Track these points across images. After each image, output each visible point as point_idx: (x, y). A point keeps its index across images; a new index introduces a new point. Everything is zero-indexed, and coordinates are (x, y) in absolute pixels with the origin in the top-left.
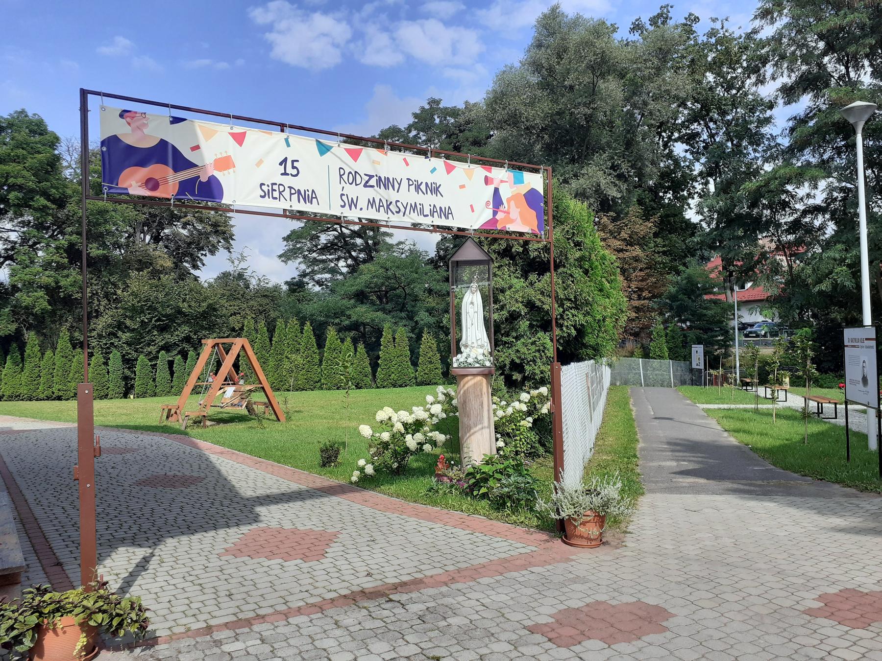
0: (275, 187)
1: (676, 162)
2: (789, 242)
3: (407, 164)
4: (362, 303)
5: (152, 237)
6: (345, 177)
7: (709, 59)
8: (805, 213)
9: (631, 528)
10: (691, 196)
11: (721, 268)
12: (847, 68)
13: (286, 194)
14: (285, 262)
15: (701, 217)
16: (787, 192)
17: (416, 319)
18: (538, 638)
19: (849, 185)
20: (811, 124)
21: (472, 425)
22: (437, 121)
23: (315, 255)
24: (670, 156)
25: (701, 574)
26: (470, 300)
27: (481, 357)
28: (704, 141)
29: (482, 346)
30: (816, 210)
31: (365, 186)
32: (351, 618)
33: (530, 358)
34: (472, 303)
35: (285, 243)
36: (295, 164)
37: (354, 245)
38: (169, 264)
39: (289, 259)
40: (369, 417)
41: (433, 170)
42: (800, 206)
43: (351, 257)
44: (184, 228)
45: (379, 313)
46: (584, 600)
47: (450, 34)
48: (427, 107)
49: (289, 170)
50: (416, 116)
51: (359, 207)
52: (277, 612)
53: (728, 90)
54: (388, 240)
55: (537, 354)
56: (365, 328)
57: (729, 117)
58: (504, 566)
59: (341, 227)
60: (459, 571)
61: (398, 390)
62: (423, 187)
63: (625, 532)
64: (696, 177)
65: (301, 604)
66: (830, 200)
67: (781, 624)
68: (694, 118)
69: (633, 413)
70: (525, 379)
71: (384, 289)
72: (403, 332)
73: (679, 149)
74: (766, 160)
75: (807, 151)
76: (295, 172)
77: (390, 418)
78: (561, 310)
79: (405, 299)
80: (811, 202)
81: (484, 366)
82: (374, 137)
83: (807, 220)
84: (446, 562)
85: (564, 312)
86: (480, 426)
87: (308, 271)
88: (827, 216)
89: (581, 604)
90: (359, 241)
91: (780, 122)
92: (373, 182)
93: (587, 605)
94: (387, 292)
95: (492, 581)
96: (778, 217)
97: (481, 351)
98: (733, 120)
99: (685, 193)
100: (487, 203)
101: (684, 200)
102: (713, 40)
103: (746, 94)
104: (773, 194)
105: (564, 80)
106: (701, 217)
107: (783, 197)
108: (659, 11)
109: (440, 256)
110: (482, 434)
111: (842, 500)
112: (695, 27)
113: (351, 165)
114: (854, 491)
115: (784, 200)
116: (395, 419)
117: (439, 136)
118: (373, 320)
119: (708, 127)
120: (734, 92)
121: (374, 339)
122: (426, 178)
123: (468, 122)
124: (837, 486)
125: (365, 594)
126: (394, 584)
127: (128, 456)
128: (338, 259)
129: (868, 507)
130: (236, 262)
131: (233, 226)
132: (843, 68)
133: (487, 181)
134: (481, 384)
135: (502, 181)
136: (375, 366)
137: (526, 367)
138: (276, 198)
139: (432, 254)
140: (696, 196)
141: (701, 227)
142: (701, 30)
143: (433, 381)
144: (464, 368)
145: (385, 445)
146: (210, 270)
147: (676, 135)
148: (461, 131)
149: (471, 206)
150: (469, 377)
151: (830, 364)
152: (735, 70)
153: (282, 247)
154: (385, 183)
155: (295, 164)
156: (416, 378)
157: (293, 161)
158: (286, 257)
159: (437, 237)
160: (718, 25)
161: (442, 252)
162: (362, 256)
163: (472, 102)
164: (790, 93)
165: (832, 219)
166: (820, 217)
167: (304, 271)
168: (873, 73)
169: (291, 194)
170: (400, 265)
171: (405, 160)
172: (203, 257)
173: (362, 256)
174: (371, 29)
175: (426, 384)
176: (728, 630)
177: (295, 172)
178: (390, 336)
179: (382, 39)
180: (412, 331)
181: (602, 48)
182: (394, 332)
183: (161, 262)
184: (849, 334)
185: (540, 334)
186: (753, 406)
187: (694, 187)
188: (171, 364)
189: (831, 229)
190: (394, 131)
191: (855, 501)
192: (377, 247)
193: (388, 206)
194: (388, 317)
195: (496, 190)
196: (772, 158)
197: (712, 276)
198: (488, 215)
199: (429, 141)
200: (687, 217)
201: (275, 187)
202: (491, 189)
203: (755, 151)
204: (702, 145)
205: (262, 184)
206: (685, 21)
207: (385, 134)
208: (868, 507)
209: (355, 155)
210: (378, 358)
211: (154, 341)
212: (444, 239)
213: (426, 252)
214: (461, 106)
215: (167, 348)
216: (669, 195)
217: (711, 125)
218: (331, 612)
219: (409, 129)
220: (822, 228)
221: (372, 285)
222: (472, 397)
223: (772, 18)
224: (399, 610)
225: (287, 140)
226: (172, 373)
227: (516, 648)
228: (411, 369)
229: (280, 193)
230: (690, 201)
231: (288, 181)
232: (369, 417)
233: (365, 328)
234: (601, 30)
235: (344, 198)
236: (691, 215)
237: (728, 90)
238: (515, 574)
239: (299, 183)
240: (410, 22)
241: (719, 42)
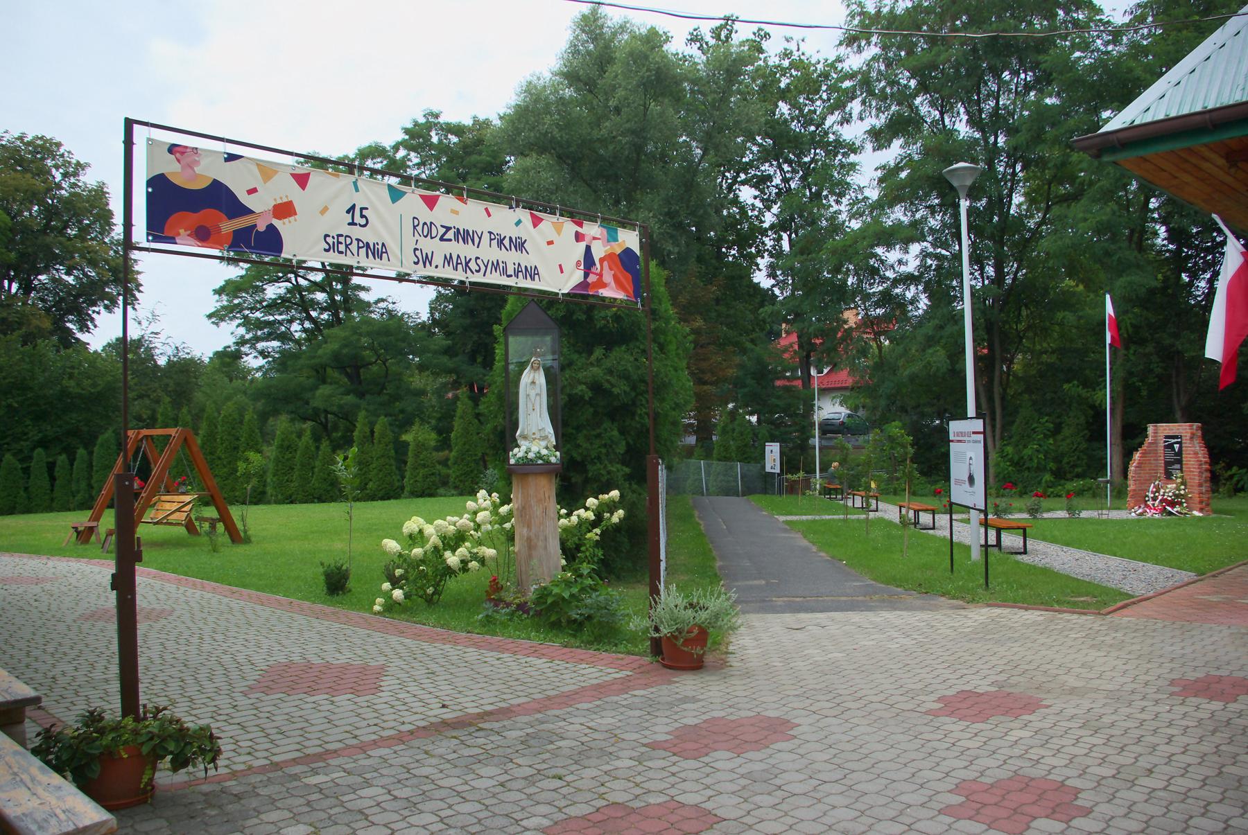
0: (342, 239)
1: (743, 209)
2: (878, 317)
3: (489, 215)
5: (20, 285)
6: (419, 228)
7: (782, 85)
8: (896, 282)
9: (731, 648)
10: (760, 254)
11: (796, 347)
12: (942, 114)
13: (354, 247)
14: (217, 324)
15: (773, 282)
16: (875, 256)
18: (662, 753)
19: (944, 252)
20: (903, 175)
22: (435, 139)
23: (258, 314)
24: (736, 201)
25: (818, 687)
27: (544, 452)
28: (777, 186)
29: (545, 438)
30: (908, 279)
31: (442, 239)
32: (444, 746)
33: (593, 454)
34: (533, 383)
35: (217, 297)
36: (365, 212)
37: (314, 304)
38: (47, 324)
39: (222, 320)
40: (394, 531)
41: (518, 223)
42: (890, 274)
43: (309, 318)
44: (68, 273)
45: (350, 398)
46: (593, 803)
49: (358, 219)
50: (407, 131)
51: (434, 264)
52: (348, 747)
53: (805, 125)
54: (363, 296)
55: (604, 451)
57: (807, 159)
58: (600, 690)
59: (297, 276)
60: (549, 698)
62: (506, 242)
63: (727, 653)
64: (766, 230)
65: (374, 737)
66: (924, 268)
67: (905, 725)
68: (766, 155)
69: (702, 527)
70: (587, 481)
73: (747, 194)
74: (852, 216)
75: (897, 208)
76: (363, 221)
78: (633, 394)
80: (903, 269)
81: (548, 463)
82: (346, 157)
83: (898, 291)
84: (531, 691)
87: (248, 337)
88: (920, 288)
89: (696, 721)
90: (320, 296)
91: (868, 170)
92: (450, 235)
93: (705, 721)
95: (590, 705)
96: (866, 286)
97: (544, 443)
98: (811, 162)
99: (753, 250)
100: (578, 263)
101: (751, 259)
102: (786, 63)
103: (826, 133)
104: (858, 252)
105: (607, 100)
106: (773, 282)
107: (872, 262)
109: (434, 320)
111: (950, 612)
112: (765, 45)
113: (425, 215)
114: (961, 602)
115: (873, 267)
117: (438, 159)
118: (341, 407)
119: (781, 170)
120: (813, 128)
122: (510, 231)
124: (943, 599)
125: (445, 724)
126: (478, 714)
127: (48, 586)
128: (291, 321)
129: (977, 617)
130: (145, 324)
131: (139, 273)
132: (937, 113)
133: (579, 237)
135: (595, 238)
137: (589, 467)
138: (341, 253)
139: (425, 316)
140: (766, 254)
141: (773, 294)
142: (773, 51)
146: (102, 331)
147: (743, 176)
149: (560, 266)
151: (932, 463)
152: (813, 101)
153: (214, 303)
154: (465, 236)
155: (365, 212)
157: (362, 209)
158: (218, 317)
159: (431, 292)
160: (792, 46)
161: (437, 315)
162: (325, 316)
163: (482, 117)
164: (880, 138)
165: (925, 291)
166: (912, 288)
167: (243, 336)
168: (967, 121)
169: (359, 248)
171: (486, 210)
172: (95, 316)
173: (325, 316)
176: (854, 733)
177: (363, 221)
181: (657, 63)
183: (35, 322)
184: (955, 427)
185: (607, 424)
186: (842, 517)
187: (763, 243)
188: (51, 467)
189: (924, 302)
190: (375, 151)
191: (963, 612)
193: (467, 264)
195: (588, 248)
196: (859, 214)
197: (786, 356)
198: (578, 276)
200: (756, 280)
201: (342, 239)
202: (583, 245)
203: (837, 202)
204: (775, 191)
205: (327, 236)
206: (753, 37)
207: (364, 154)
208: (977, 617)
209: (431, 202)
211: (25, 434)
212: (440, 297)
215: (44, 443)
216: (733, 252)
217: (786, 167)
218: (415, 743)
219: (396, 148)
220: (914, 301)
223: (859, 47)
224: (495, 738)
225: (355, 183)
226: (53, 479)
227: (640, 763)
229: (347, 246)
230: (759, 260)
231: (356, 232)
232: (394, 531)
234: (653, 40)
235: (418, 253)
236: (761, 278)
237: (805, 125)
238: (615, 698)
239: (367, 235)
241: (793, 65)
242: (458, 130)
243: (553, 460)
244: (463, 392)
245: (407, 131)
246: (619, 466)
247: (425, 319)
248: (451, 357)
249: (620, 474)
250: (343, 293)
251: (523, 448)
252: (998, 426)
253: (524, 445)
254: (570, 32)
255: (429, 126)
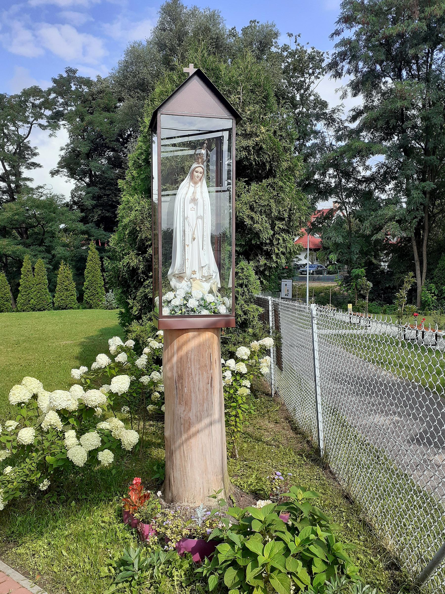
4: (5, 237)
17: (53, 252)
21: (193, 418)
22: (73, 88)
26: (190, 195)
29: (208, 279)
45: (20, 247)
47: (79, 39)
48: (65, 75)
54: (28, 183)
56: (6, 259)
61: (37, 314)
71: (24, 225)
72: (41, 264)
77: (35, 397)
78: (272, 232)
79: (44, 235)
81: (216, 314)
85: (274, 234)
86: (206, 421)
94: (27, 229)
97: (207, 286)
108: (249, 24)
109: (74, 202)
110: (210, 434)
116: (44, 401)
117: (75, 100)
118: (14, 252)
121: (15, 269)
123: (100, 92)
134: (210, 347)
136: (15, 292)
139: (68, 199)
143: (69, 305)
144: (182, 316)
145: (25, 450)
148: (94, 99)
150: (191, 334)
156: (53, 303)
161: (76, 199)
170: (39, 205)
174: (17, 25)
175: (63, 309)
178: (30, 267)
179: (26, 35)
180: (49, 263)
182: (34, 263)
192: (19, 189)
194: (28, 250)
199: (66, 104)
210: (19, 285)
213: (63, 196)
214: (94, 79)
219: (49, 92)
221: (14, 222)
222: (194, 369)
228: (49, 296)
233: (6, 259)
240: (50, 25)
241: (292, 54)
242: (88, 82)
243: (223, 310)
244: (92, 245)
245: (55, 81)
246: (255, 306)
247: (69, 201)
248: (85, 224)
249: (256, 314)
250: (16, 182)
251: (181, 293)
252: (425, 271)
253: (181, 287)
254: (159, 15)
255: (68, 80)
